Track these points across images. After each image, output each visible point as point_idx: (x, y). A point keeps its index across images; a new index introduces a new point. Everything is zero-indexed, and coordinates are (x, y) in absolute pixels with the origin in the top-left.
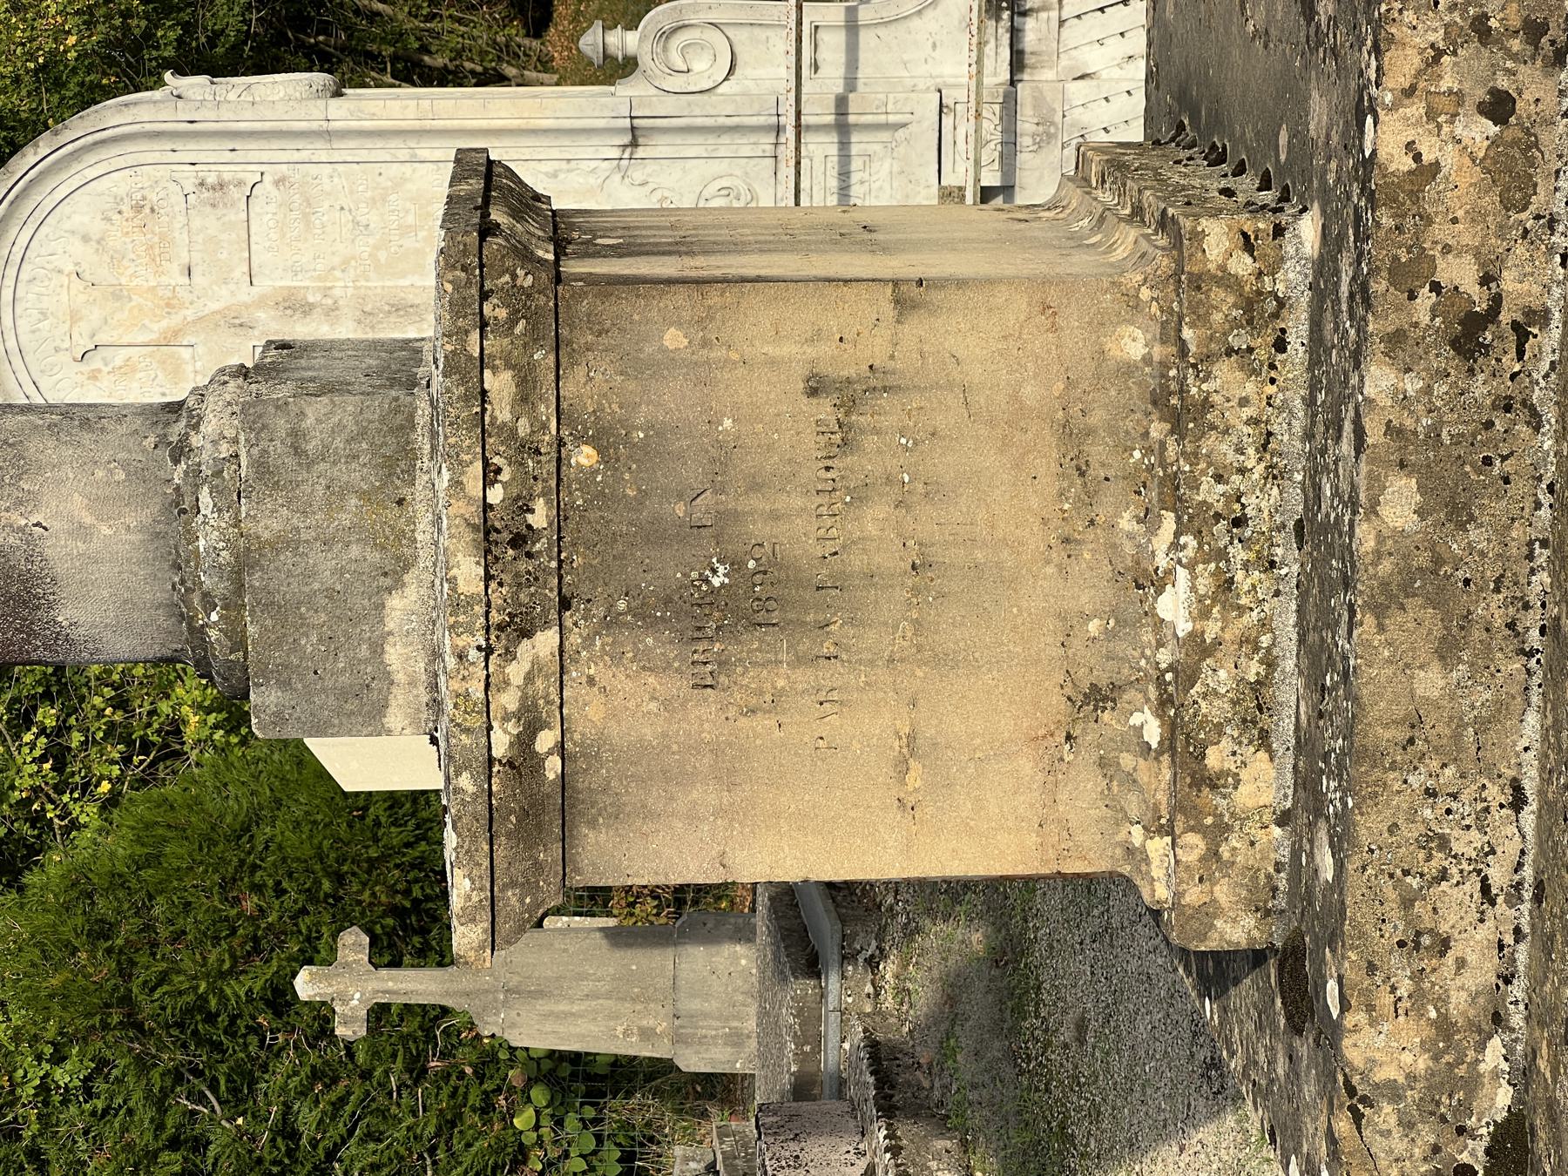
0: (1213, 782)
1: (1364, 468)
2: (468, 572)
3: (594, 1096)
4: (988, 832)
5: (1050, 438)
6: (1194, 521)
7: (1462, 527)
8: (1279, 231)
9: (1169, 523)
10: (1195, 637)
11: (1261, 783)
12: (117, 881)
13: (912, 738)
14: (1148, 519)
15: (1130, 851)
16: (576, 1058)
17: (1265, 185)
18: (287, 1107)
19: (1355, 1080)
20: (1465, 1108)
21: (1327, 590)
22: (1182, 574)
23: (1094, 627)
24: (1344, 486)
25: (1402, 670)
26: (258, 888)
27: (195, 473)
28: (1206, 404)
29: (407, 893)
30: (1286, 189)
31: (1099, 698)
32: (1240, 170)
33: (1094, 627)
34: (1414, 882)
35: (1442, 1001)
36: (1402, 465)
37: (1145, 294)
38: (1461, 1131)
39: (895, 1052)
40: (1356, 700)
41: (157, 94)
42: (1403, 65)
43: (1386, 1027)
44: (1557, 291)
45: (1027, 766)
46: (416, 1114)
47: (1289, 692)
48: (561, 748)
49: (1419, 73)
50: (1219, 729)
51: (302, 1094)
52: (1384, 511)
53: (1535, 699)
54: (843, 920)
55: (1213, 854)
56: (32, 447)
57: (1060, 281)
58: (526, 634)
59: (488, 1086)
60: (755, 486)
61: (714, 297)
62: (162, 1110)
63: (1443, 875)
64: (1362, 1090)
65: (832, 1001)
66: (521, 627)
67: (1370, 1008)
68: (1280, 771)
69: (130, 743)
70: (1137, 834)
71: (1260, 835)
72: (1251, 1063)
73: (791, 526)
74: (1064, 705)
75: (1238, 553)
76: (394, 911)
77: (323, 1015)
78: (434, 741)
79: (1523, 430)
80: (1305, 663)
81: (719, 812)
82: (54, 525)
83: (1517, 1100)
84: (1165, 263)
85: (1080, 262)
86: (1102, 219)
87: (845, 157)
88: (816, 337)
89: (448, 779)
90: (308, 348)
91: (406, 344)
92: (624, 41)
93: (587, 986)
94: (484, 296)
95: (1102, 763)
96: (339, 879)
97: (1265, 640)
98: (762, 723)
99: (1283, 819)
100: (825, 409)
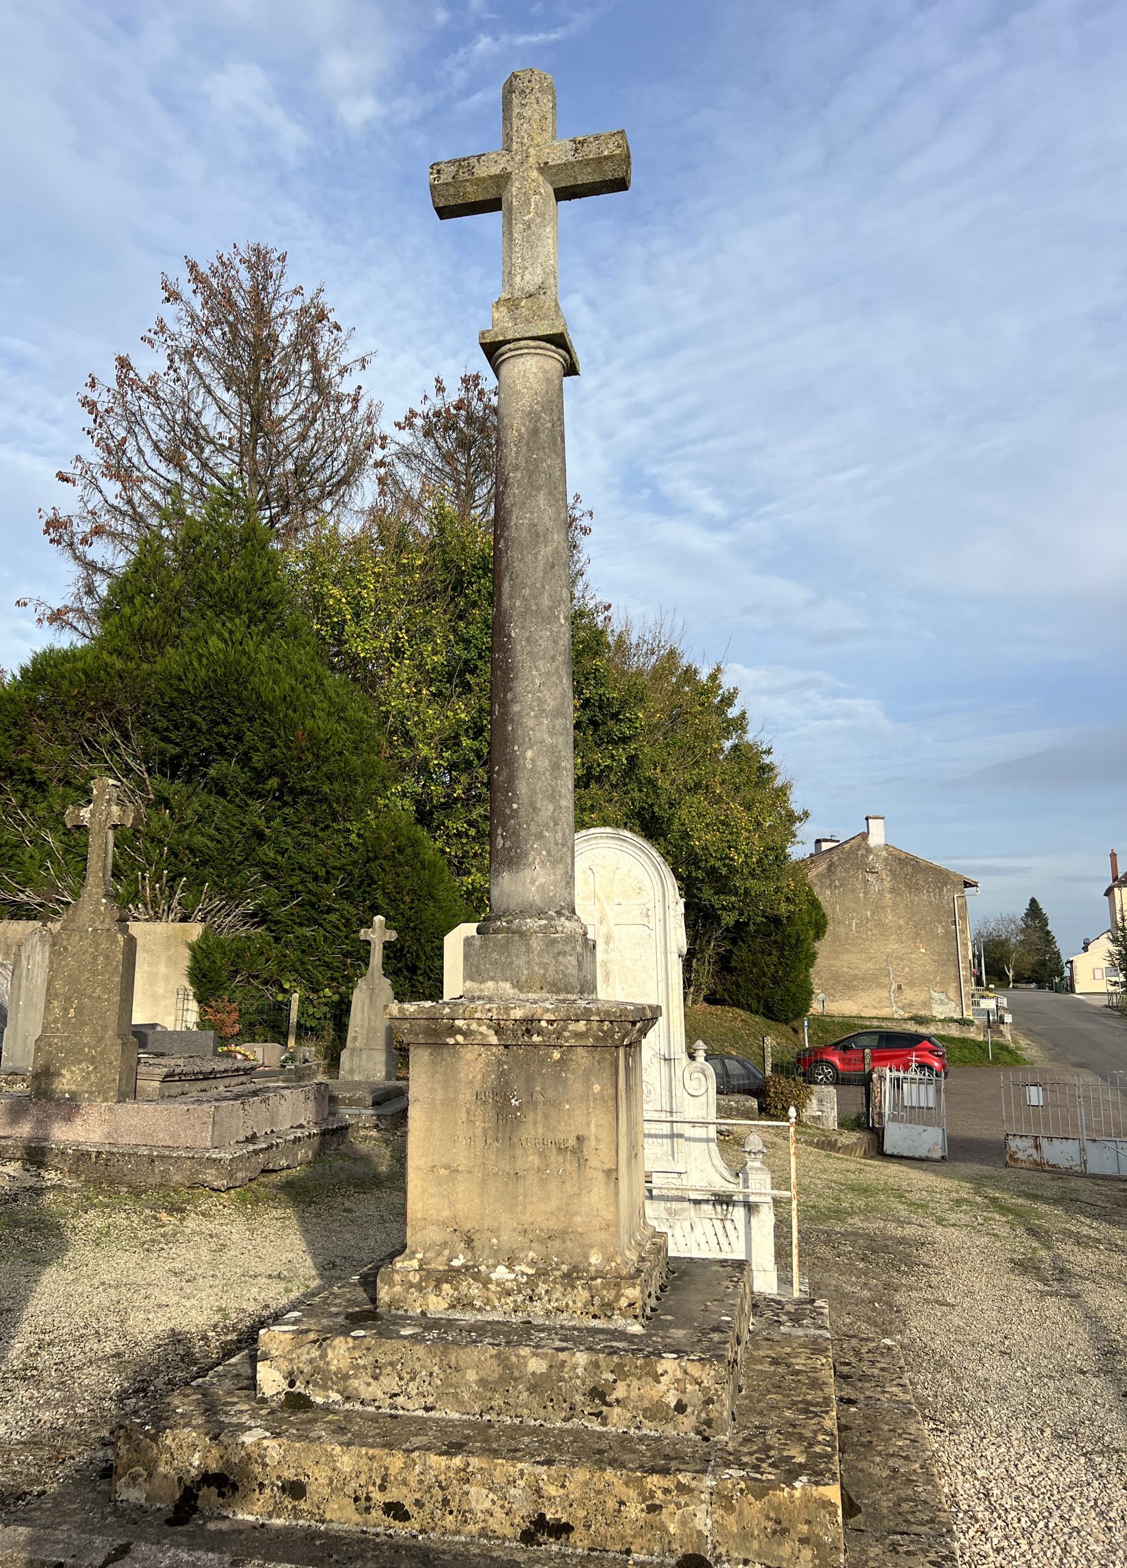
0: (437, 1287)
1: (550, 1351)
2: (518, 1014)
3: (335, 1017)
4: (422, 1196)
5: (562, 1226)
6: (532, 1281)
7: (528, 1390)
8: (636, 1317)
9: (531, 1271)
10: (490, 1281)
11: (437, 1305)
12: (417, 855)
13: (457, 1171)
14: (533, 1263)
15: (414, 1253)
16: (348, 1010)
17: (653, 1310)
18: (337, 910)
19: (328, 1342)
20: (316, 1384)
21: (507, 1334)
22: (513, 1276)
23: (494, 1241)
24: (543, 1343)
25: (477, 1363)
26: (412, 901)
27: (552, 919)
28: (574, 1287)
29: (408, 952)
30: (651, 1319)
31: (469, 1242)
32: (658, 1299)
33: (494, 1241)
34: (399, 1367)
35: (356, 1376)
36: (551, 1366)
37: (613, 1264)
38: (308, 1383)
39: (344, 1136)
40: (466, 1346)
41: (678, 896)
42: (695, 1370)
43: (347, 1354)
44: (613, 1429)
45: (446, 1213)
46: (332, 955)
47: (469, 1317)
48: (457, 1044)
49: (692, 1376)
50: (456, 1289)
51: (342, 916)
52: (534, 1360)
53: (465, 1417)
54: (392, 1115)
55: (412, 1286)
56: (561, 866)
57: (618, 1232)
58: (496, 1033)
59: (340, 979)
60: (546, 1116)
61: (611, 1103)
62: (339, 869)
63: (401, 1379)
64: (324, 1344)
65: (363, 1111)
66: (499, 1031)
67: (354, 1348)
68: (440, 1312)
69: (462, 857)
70: (419, 1256)
71: (418, 1304)
72: (336, 1296)
73: (532, 1129)
74: (467, 1229)
75: (520, 1298)
76: (402, 947)
77: (368, 924)
78: (461, 997)
79: (563, 1415)
80: (480, 1324)
81: (434, 1100)
82: (535, 873)
83: (318, 1405)
84: (624, 1272)
85: (624, 1238)
86: (640, 1245)
87: (662, 1136)
88: (598, 1140)
89: (448, 1004)
90: (594, 955)
91: (595, 988)
92: (701, 1055)
93: (373, 1018)
94: (611, 1022)
95: (446, 1243)
96: (414, 929)
97: (488, 1308)
98: (464, 1116)
99: (423, 1313)
100: (572, 1142)
